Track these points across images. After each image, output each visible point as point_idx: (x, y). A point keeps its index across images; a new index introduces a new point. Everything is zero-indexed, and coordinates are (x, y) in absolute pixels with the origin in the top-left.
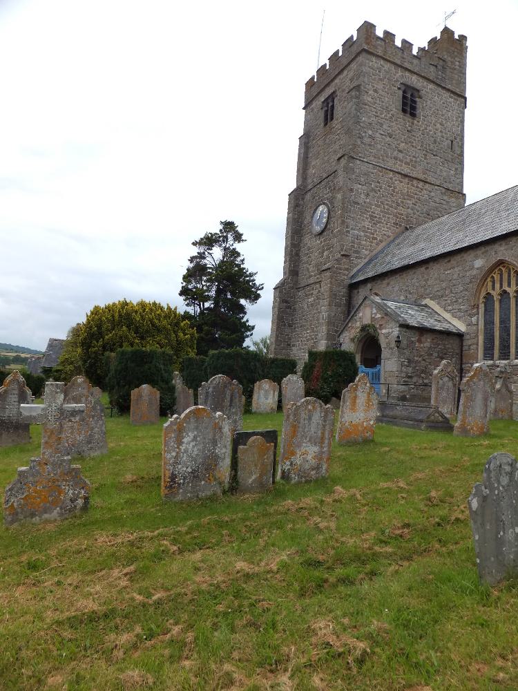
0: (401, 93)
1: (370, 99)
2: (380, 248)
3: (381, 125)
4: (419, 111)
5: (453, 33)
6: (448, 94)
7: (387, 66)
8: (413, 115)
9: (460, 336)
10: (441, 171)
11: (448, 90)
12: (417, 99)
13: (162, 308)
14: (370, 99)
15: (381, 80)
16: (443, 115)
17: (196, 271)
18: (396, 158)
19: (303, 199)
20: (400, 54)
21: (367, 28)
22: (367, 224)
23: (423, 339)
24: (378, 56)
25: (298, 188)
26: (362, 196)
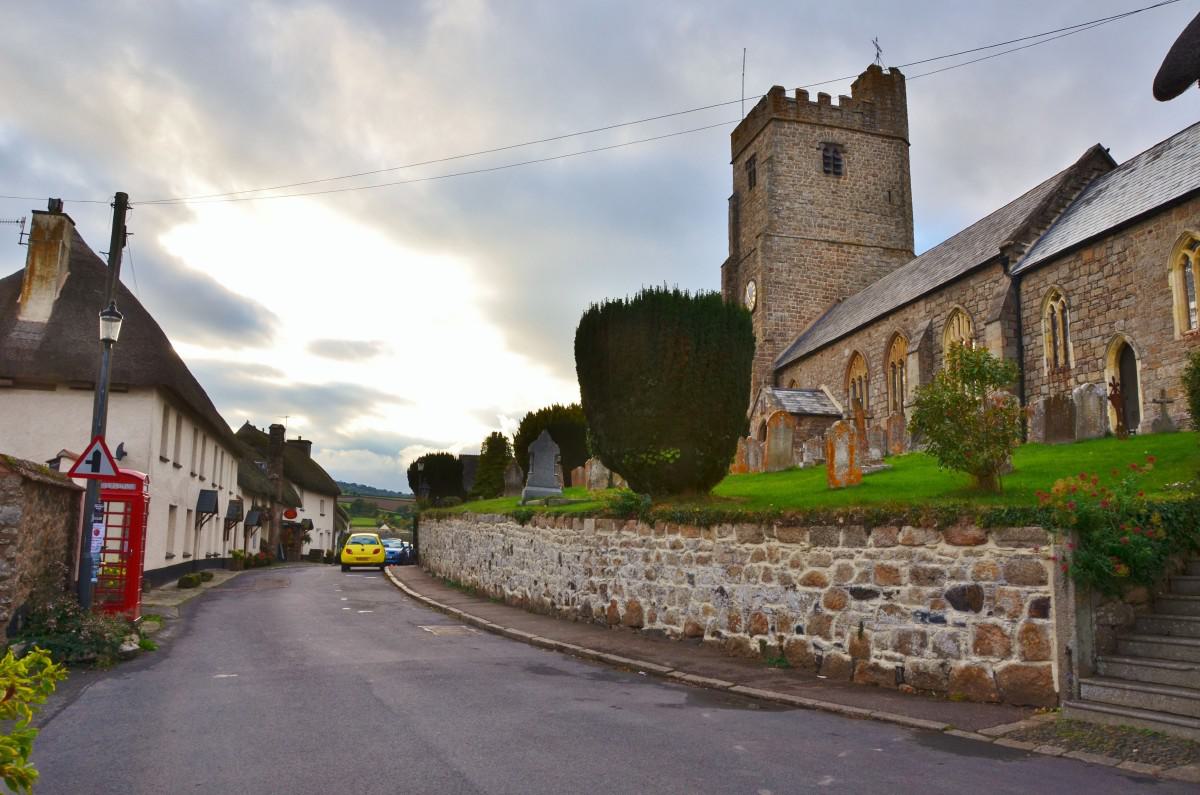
0: (820, 153)
1: (785, 168)
3: (800, 193)
4: (846, 168)
5: (880, 69)
8: (838, 174)
11: (879, 135)
18: (820, 226)
19: (736, 271)
23: (803, 423)
24: (789, 121)
26: (784, 274)
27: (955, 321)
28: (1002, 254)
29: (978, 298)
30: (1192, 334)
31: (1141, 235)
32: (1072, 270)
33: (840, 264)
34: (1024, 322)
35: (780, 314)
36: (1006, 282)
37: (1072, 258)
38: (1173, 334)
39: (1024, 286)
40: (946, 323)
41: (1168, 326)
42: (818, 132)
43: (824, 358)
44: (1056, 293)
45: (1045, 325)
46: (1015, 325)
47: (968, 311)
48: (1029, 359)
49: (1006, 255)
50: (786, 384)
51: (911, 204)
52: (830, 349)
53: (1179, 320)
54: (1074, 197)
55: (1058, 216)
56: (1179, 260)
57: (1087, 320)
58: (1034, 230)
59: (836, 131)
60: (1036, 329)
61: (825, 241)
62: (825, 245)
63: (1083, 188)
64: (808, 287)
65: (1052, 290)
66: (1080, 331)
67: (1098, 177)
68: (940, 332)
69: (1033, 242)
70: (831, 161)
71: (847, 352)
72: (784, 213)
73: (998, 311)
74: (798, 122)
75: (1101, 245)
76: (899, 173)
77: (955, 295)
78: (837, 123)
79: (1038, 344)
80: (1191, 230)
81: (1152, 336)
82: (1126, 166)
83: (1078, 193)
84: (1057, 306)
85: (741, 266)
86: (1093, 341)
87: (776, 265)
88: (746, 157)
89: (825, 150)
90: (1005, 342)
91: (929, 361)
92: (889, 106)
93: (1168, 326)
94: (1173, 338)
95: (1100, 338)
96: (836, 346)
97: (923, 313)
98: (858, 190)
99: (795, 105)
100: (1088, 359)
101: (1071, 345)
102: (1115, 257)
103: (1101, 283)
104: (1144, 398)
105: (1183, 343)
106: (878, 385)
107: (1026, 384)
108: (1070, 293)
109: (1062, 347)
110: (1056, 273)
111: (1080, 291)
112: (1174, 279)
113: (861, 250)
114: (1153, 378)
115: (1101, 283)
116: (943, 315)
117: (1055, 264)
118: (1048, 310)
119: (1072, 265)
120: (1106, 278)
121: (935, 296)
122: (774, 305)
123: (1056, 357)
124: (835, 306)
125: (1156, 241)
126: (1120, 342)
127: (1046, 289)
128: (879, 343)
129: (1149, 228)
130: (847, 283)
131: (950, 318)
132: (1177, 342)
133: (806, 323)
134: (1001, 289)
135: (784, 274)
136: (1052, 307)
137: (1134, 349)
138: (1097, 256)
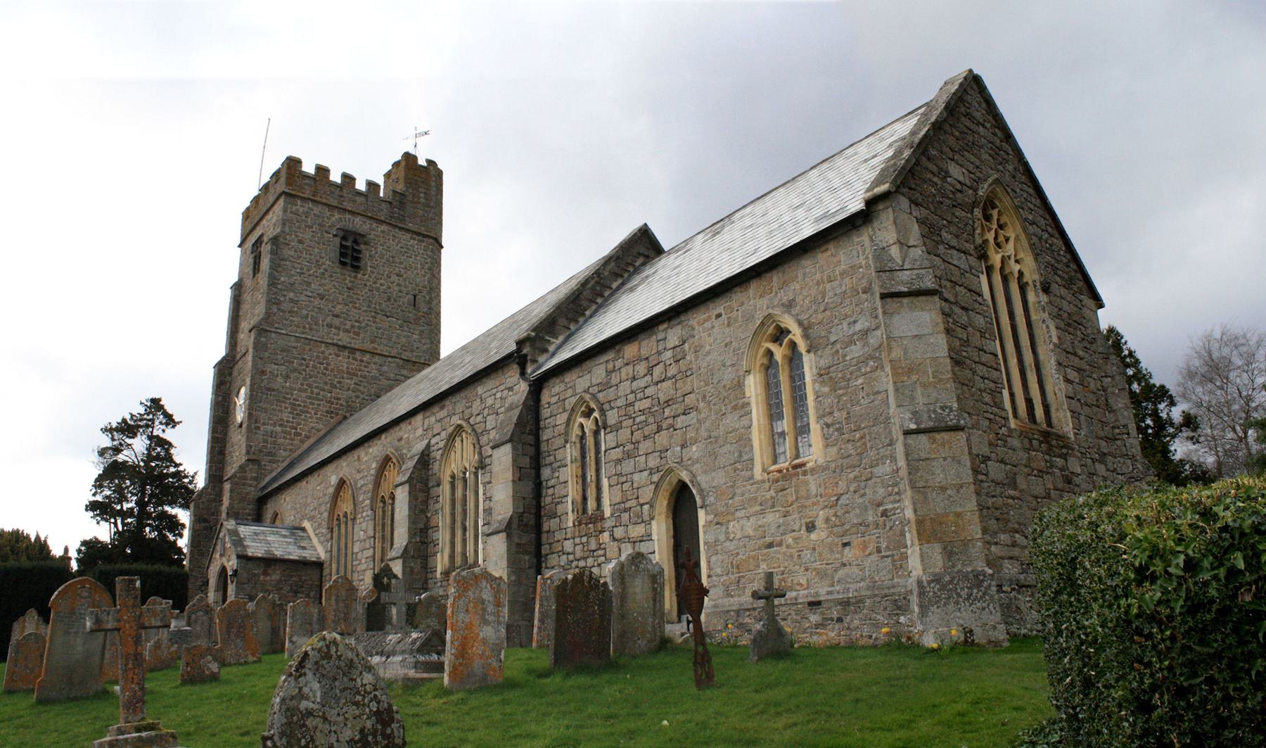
0: (338, 240)
1: (292, 253)
2: (306, 446)
3: (309, 284)
4: (366, 262)
5: (415, 158)
6: (408, 236)
7: (317, 210)
8: (356, 268)
9: (319, 565)
10: (398, 336)
11: (408, 231)
12: (363, 247)
13: (28, 537)
14: (292, 253)
15: (310, 227)
16: (401, 263)
17: (113, 472)
18: (330, 326)
19: (230, 374)
20: (337, 192)
21: (292, 164)
22: (285, 416)
23: (270, 571)
24: (303, 199)
25: (227, 355)
26: (280, 379)
27: (458, 443)
28: (519, 350)
29: (486, 412)
30: (780, 471)
31: (706, 321)
32: (609, 373)
33: (351, 375)
34: (544, 447)
35: (270, 428)
36: (523, 388)
37: (610, 355)
38: (752, 469)
39: (545, 397)
40: (446, 446)
41: (745, 457)
42: (337, 216)
43: (310, 486)
44: (588, 406)
45: (570, 452)
46: (531, 451)
47: (474, 430)
48: (548, 500)
49: (525, 351)
50: (268, 516)
51: (438, 314)
52: (316, 474)
53: (761, 449)
54: (614, 285)
55: (594, 307)
56: (761, 359)
57: (629, 447)
58: (562, 321)
59: (358, 219)
60: (559, 457)
61: (333, 344)
62: (333, 350)
63: (626, 275)
64: (309, 398)
65: (582, 401)
66: (619, 461)
67: (644, 264)
68: (438, 457)
69: (561, 338)
70: (350, 252)
71: (334, 480)
72: (285, 306)
73: (510, 428)
74: (313, 201)
75: (651, 336)
76: (428, 276)
77: (460, 407)
78: (361, 209)
79: (562, 480)
80: (776, 312)
81: (721, 473)
82: (675, 250)
83: (620, 281)
84: (589, 425)
85: (236, 367)
86: (636, 477)
87: (271, 368)
88: (252, 239)
89: (344, 238)
90: (517, 475)
91: (421, 496)
92: (422, 200)
93: (745, 457)
94: (752, 477)
95: (646, 473)
96: (322, 472)
97: (420, 432)
98: (378, 289)
99: (312, 182)
100: (628, 505)
101: (605, 482)
102: (669, 354)
103: (649, 391)
104: (710, 568)
105: (767, 485)
106: (364, 526)
107: (544, 536)
108: (606, 407)
109: (594, 485)
110: (588, 376)
111: (620, 403)
112: (753, 386)
113: (376, 359)
114: (722, 537)
115: (649, 391)
116: (444, 434)
117: (588, 364)
118: (576, 431)
119: (610, 366)
120: (657, 384)
121: (436, 409)
122: (262, 416)
123: (585, 499)
124: (340, 422)
125: (727, 330)
126: (675, 481)
127: (573, 400)
128: (369, 469)
129: (716, 312)
130: (357, 397)
131: (451, 439)
132: (757, 483)
133: (302, 442)
134: (516, 398)
135: (280, 379)
136: (582, 426)
137: (694, 492)
138: (645, 352)
